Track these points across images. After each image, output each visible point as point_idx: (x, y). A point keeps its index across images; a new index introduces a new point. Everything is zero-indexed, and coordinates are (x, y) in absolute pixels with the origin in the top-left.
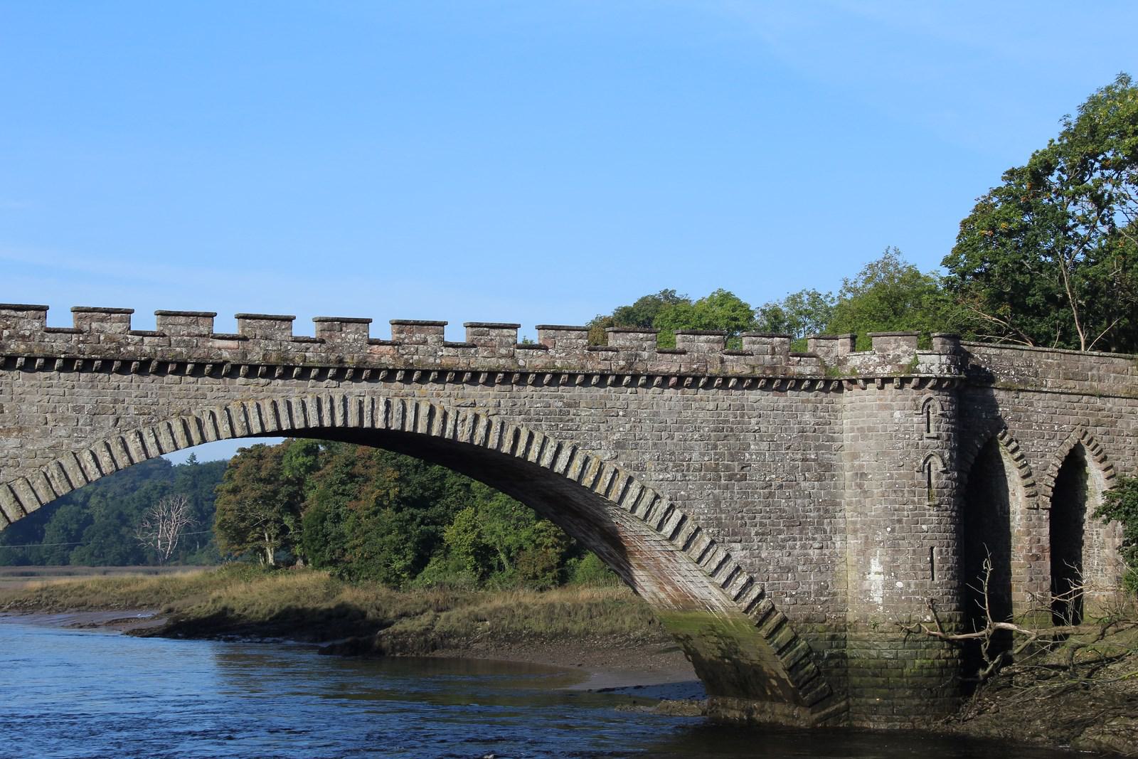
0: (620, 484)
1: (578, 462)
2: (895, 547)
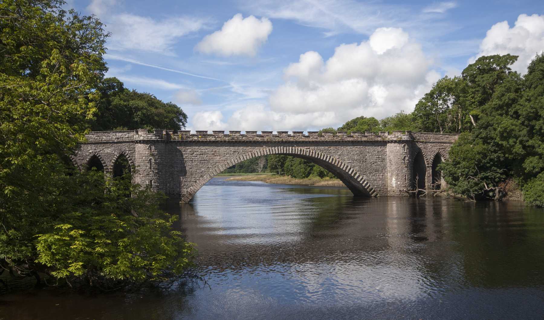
0: (340, 164)
1: (331, 159)
2: (397, 175)
